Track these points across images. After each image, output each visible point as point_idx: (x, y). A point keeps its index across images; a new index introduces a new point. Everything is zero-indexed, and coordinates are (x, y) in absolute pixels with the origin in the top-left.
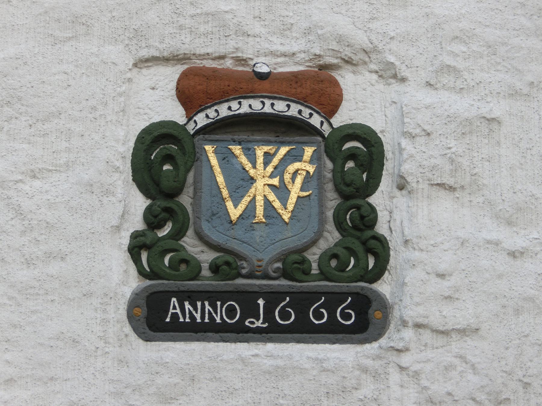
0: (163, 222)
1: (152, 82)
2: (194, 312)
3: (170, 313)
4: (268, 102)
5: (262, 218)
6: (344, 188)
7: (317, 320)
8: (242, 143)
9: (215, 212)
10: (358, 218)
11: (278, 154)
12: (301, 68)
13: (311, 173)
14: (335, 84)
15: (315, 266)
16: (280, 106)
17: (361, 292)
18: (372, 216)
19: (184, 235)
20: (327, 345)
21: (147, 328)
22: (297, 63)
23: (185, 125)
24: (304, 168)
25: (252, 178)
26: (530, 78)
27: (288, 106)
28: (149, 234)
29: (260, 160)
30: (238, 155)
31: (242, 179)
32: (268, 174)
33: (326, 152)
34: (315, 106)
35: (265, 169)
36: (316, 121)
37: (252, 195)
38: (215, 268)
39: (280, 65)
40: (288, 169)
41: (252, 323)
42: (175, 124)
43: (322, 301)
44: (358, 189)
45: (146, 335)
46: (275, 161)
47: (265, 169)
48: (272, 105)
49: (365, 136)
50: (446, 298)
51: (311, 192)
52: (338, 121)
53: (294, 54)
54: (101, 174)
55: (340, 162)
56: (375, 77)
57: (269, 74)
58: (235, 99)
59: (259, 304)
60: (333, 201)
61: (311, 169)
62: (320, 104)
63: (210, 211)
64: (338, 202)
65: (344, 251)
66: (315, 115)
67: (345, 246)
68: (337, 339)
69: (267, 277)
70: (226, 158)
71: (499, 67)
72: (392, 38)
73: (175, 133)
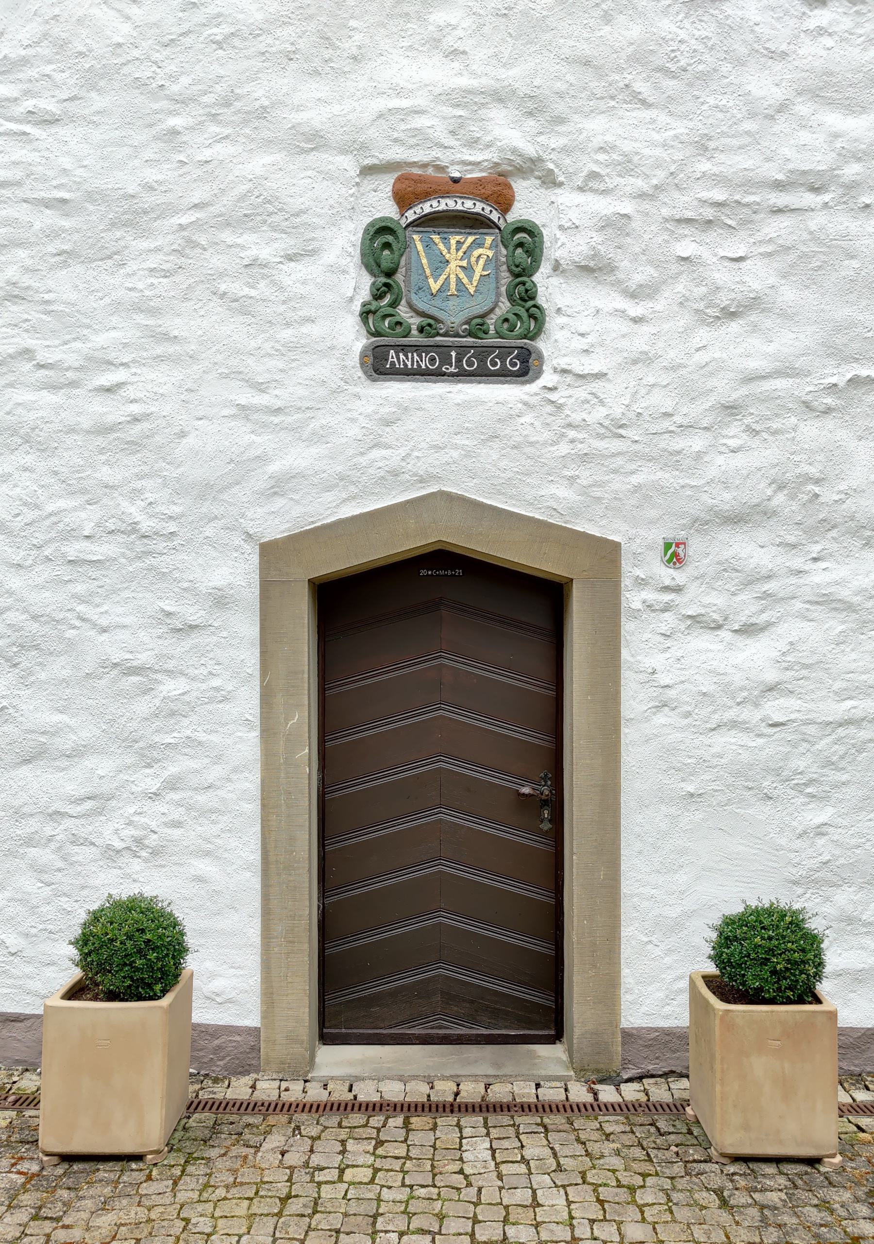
4: (460, 201)
6: (514, 268)
12: (484, 174)
14: (510, 187)
15: (492, 327)
16: (469, 204)
18: (534, 290)
19: (399, 304)
22: (481, 171)
25: (448, 261)
26: (655, 182)
28: (375, 303)
29: (453, 247)
33: (502, 241)
36: (495, 216)
42: (391, 219)
44: (524, 270)
46: (465, 247)
50: (584, 351)
52: (511, 217)
53: (479, 163)
55: (511, 248)
56: (538, 182)
57: (460, 178)
60: (506, 278)
61: (490, 254)
69: (457, 335)
70: (429, 245)
71: (632, 173)
72: (553, 149)
73: (392, 226)
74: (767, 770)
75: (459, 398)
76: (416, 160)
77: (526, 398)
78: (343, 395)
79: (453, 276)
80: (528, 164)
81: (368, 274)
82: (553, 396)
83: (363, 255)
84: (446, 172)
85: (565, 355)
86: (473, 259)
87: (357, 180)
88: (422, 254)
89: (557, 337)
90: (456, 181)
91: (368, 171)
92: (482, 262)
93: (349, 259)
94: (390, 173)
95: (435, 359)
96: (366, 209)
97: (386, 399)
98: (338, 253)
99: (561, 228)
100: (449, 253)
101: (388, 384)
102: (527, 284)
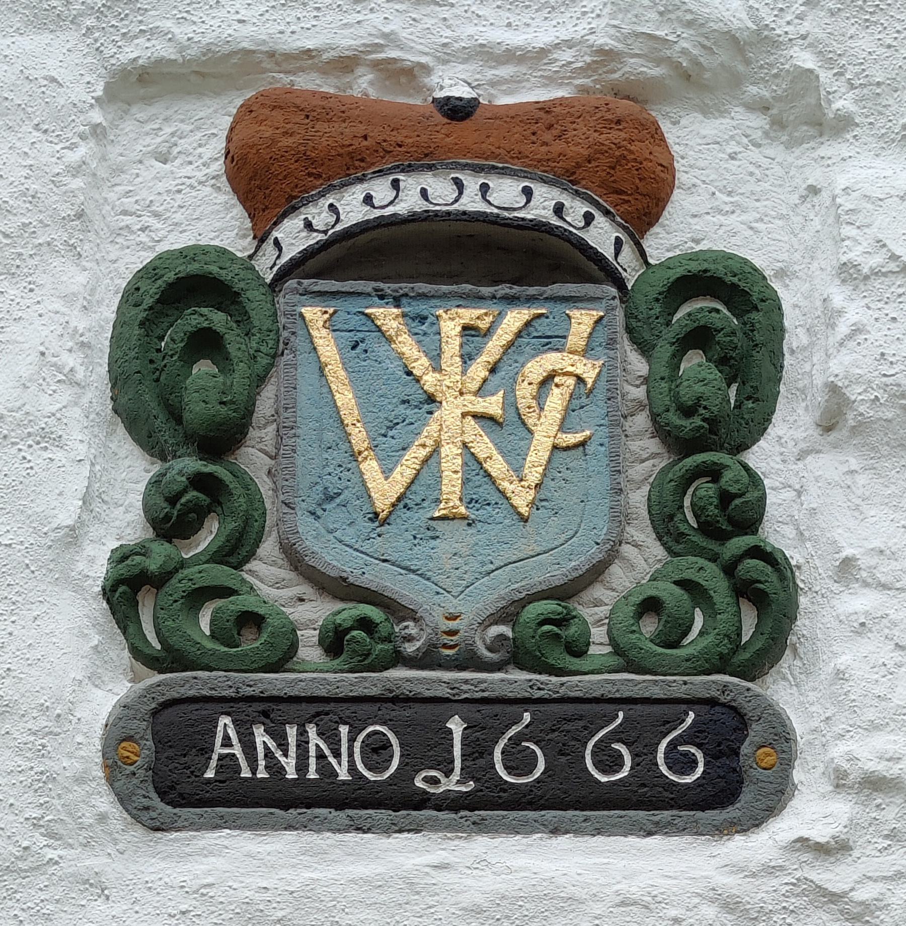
0: (193, 515)
1: (159, 140)
2: (278, 754)
3: (215, 757)
4: (472, 184)
5: (458, 503)
6: (675, 419)
7: (604, 772)
8: (404, 301)
9: (332, 491)
10: (716, 501)
11: (499, 331)
13: (590, 382)
15: (598, 634)
16: (506, 193)
17: (722, 699)
19: (251, 555)
20: (632, 840)
21: (154, 795)
22: (551, 81)
23: (251, 257)
24: (570, 369)
25: (431, 399)
27: (528, 192)
29: (452, 346)
30: (392, 332)
31: (404, 402)
32: (474, 386)
33: (629, 330)
34: (600, 197)
35: (464, 373)
36: (602, 236)
37: (429, 442)
38: (334, 642)
39: (504, 87)
40: (526, 370)
41: (435, 781)
43: (619, 721)
44: (713, 423)
45: (154, 814)
46: (493, 347)
47: (464, 373)
48: (484, 188)
49: (735, 280)
51: (588, 433)
53: (543, 52)
54: (25, 387)
55: (664, 351)
56: (757, 122)
58: (381, 173)
59: (450, 732)
60: (646, 457)
61: (589, 371)
62: (613, 190)
63: (319, 488)
64: (662, 465)
65: (678, 591)
66: (600, 220)
67: (677, 578)
68: (657, 823)
69: (469, 661)
70: (360, 342)
73: (224, 275)
74: (518, 613)
75: (479, 886)
76: (310, 44)
77: (729, 882)
78: (42, 881)
79: (451, 460)
80: (723, 56)
81: (137, 450)
82: (835, 876)
83: (118, 379)
84: (420, 89)
85: (874, 727)
86: (525, 393)
87: (96, 116)
88: (336, 372)
89: (843, 660)
90: (457, 111)
91: (139, 85)
92: (556, 399)
93: (66, 395)
94: (217, 94)
95: (387, 745)
96: (128, 220)
97: (201, 892)
98: (25, 372)
99: (848, 273)
100: (437, 369)
101: (210, 838)
102: (727, 476)
